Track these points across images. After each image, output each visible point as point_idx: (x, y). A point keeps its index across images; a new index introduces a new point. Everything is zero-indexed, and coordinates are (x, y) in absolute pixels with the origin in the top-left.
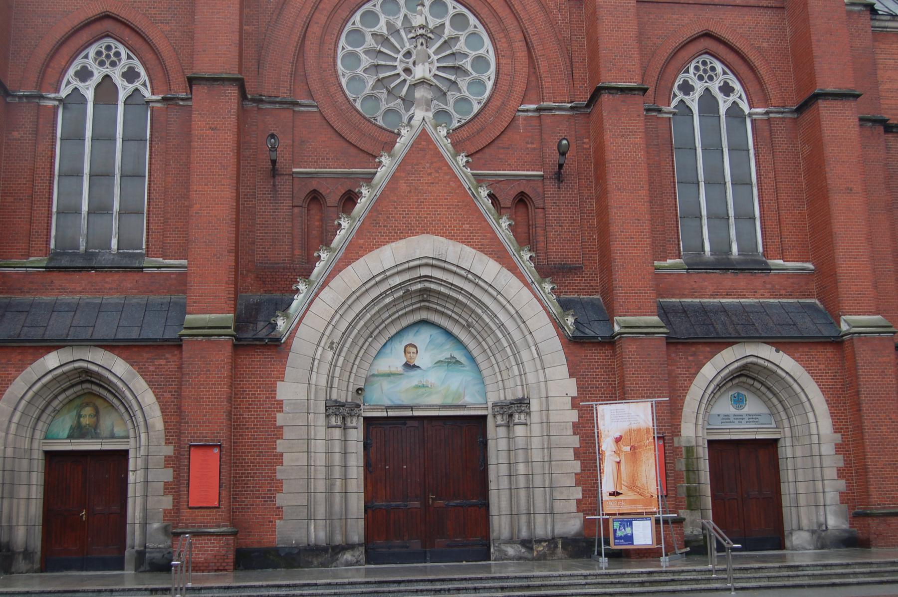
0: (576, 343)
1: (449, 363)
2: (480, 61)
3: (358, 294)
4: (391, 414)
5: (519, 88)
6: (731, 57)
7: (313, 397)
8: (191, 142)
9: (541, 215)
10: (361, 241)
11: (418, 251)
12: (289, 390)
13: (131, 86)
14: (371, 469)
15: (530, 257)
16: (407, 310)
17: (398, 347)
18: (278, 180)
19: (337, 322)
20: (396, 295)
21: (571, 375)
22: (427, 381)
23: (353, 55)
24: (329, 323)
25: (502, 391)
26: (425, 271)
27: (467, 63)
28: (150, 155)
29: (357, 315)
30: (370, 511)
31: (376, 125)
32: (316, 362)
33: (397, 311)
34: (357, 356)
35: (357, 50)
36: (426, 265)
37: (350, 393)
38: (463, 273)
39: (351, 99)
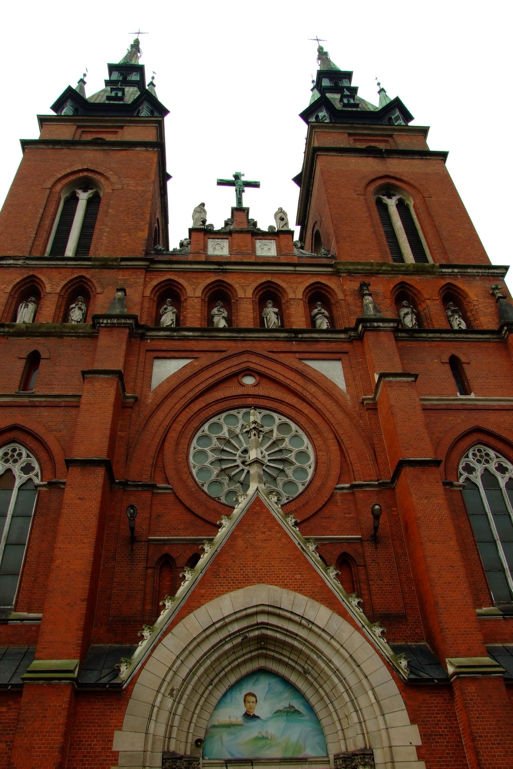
0: (410, 687)
2: (302, 455)
3: (198, 640)
5: (335, 472)
6: (499, 445)
7: (149, 748)
8: (62, 508)
9: (363, 572)
10: (203, 591)
13: (26, 476)
15: (359, 603)
16: (246, 657)
17: (239, 696)
19: (178, 668)
20: (235, 642)
22: (267, 732)
23: (202, 452)
24: (170, 669)
25: (342, 742)
26: (262, 619)
27: (292, 456)
28: (32, 527)
29: (198, 662)
31: (220, 503)
32: (156, 709)
33: (237, 659)
34: (197, 704)
35: (205, 449)
36: (263, 612)
37: (189, 745)
38: (297, 618)
39: (200, 484)
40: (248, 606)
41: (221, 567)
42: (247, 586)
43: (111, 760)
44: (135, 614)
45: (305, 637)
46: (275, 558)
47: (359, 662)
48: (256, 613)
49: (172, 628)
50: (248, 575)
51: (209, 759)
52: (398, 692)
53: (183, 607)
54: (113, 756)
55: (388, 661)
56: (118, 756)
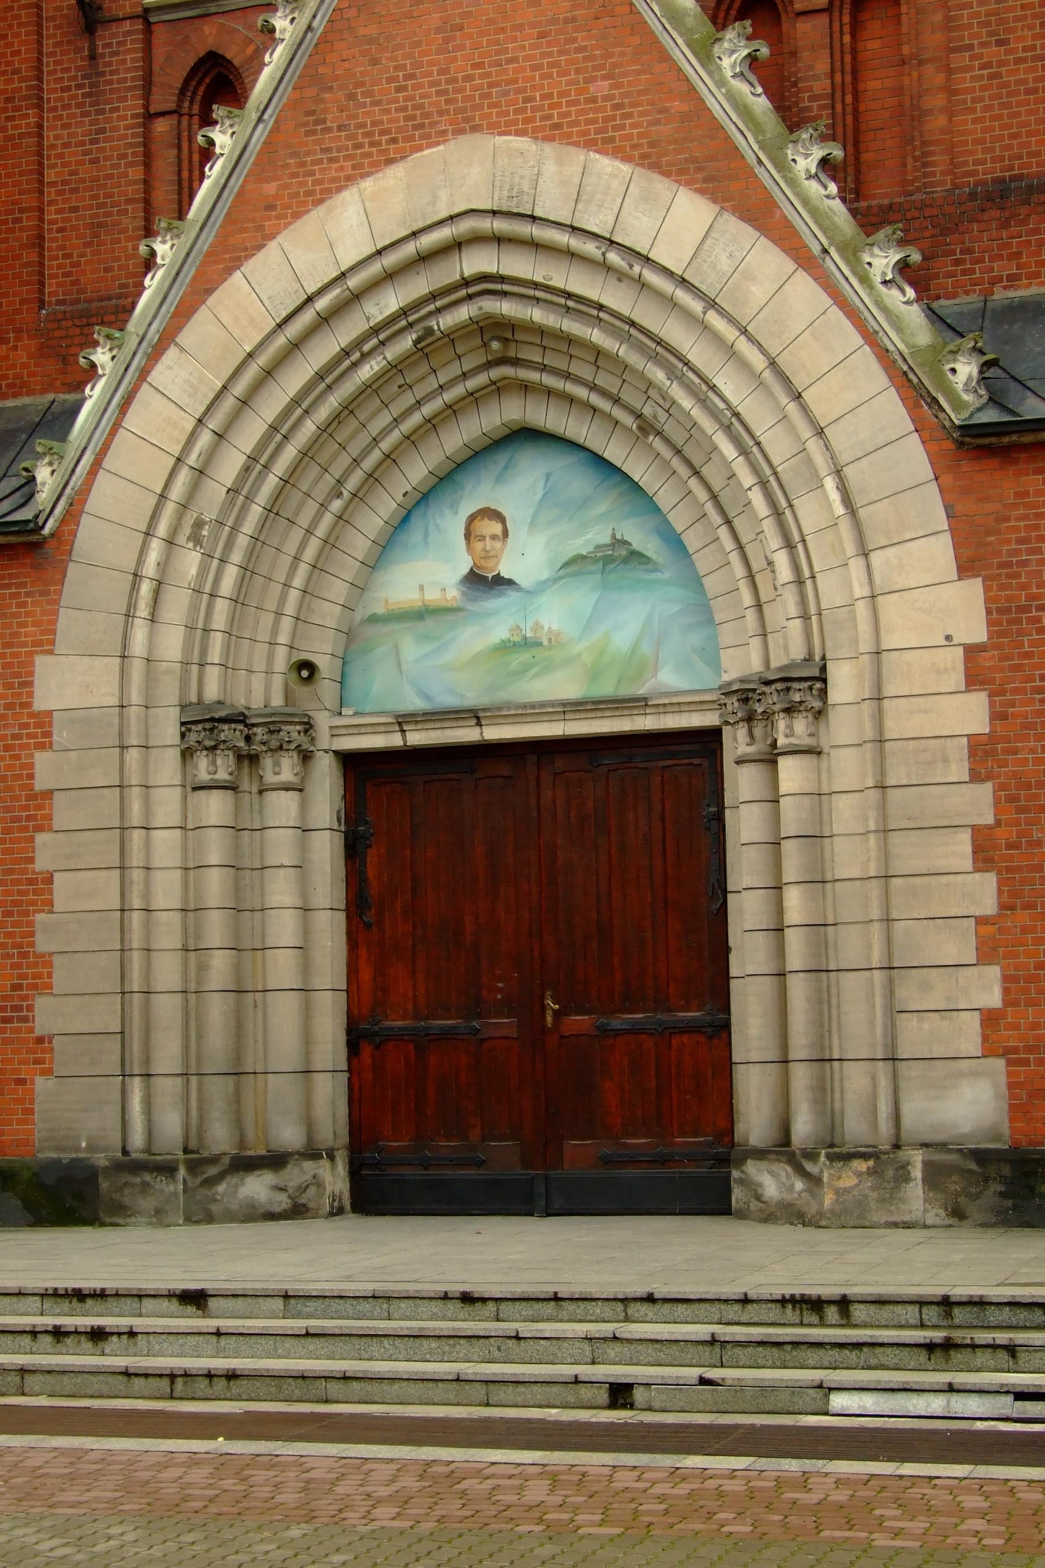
1: (607, 561)
3: (263, 360)
4: (417, 738)
10: (271, 188)
11: (444, 196)
12: (69, 681)
14: (369, 917)
17: (450, 523)
18: (105, 37)
21: (965, 569)
22: (537, 627)
26: (478, 262)
30: (366, 1051)
32: (146, 588)
34: (297, 559)
36: (478, 239)
38: (590, 248)
40: (420, 225)
41: (331, 89)
42: (420, 149)
43: (34, 736)
44: (122, 286)
45: (625, 311)
46: (520, 27)
47: (799, 381)
48: (457, 245)
49: (179, 329)
50: (421, 107)
51: (356, 714)
52: (926, 471)
53: (208, 254)
54: (38, 725)
55: (905, 368)
56: (51, 724)
